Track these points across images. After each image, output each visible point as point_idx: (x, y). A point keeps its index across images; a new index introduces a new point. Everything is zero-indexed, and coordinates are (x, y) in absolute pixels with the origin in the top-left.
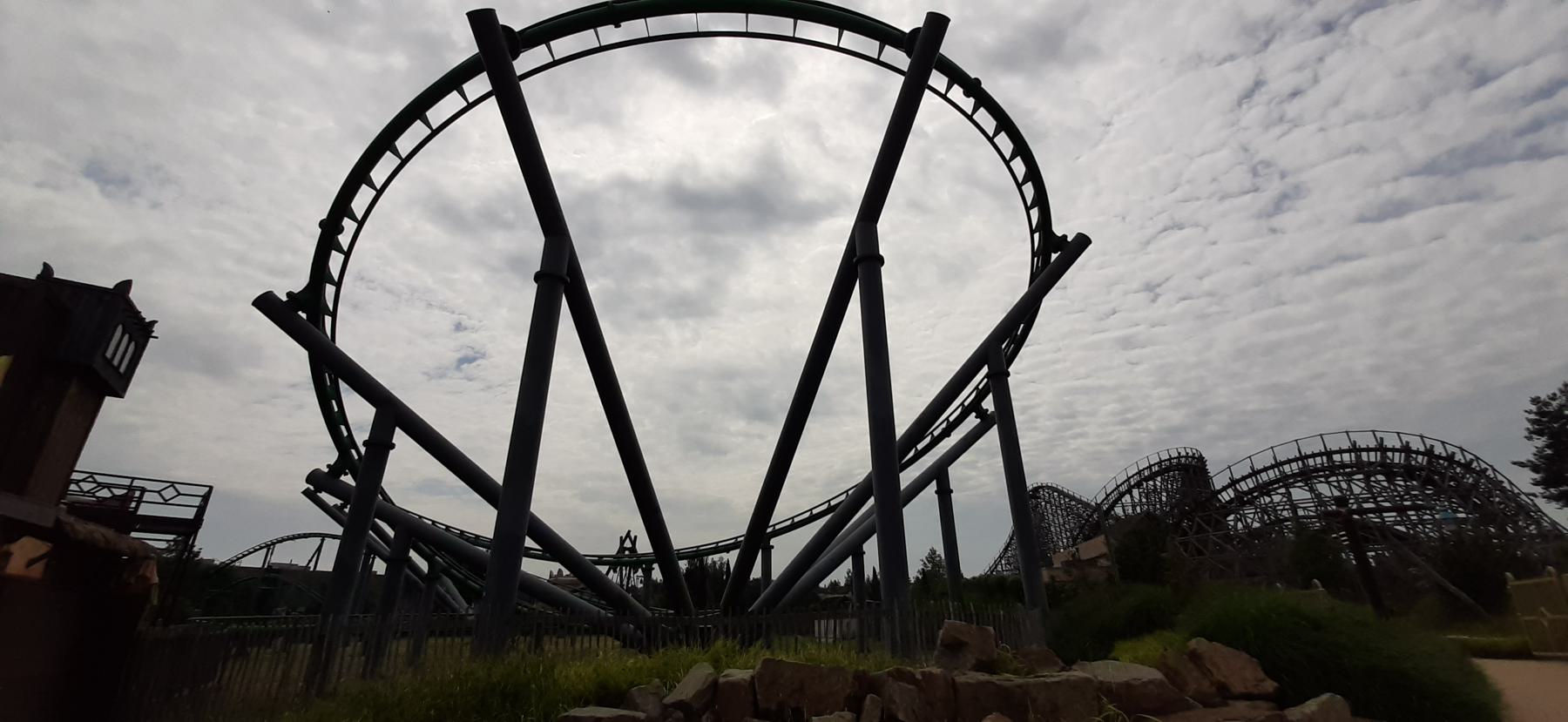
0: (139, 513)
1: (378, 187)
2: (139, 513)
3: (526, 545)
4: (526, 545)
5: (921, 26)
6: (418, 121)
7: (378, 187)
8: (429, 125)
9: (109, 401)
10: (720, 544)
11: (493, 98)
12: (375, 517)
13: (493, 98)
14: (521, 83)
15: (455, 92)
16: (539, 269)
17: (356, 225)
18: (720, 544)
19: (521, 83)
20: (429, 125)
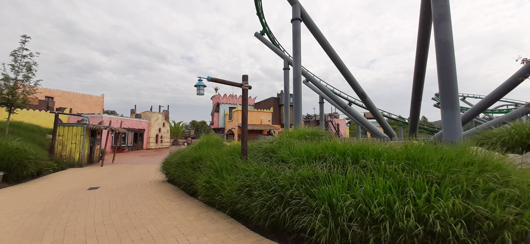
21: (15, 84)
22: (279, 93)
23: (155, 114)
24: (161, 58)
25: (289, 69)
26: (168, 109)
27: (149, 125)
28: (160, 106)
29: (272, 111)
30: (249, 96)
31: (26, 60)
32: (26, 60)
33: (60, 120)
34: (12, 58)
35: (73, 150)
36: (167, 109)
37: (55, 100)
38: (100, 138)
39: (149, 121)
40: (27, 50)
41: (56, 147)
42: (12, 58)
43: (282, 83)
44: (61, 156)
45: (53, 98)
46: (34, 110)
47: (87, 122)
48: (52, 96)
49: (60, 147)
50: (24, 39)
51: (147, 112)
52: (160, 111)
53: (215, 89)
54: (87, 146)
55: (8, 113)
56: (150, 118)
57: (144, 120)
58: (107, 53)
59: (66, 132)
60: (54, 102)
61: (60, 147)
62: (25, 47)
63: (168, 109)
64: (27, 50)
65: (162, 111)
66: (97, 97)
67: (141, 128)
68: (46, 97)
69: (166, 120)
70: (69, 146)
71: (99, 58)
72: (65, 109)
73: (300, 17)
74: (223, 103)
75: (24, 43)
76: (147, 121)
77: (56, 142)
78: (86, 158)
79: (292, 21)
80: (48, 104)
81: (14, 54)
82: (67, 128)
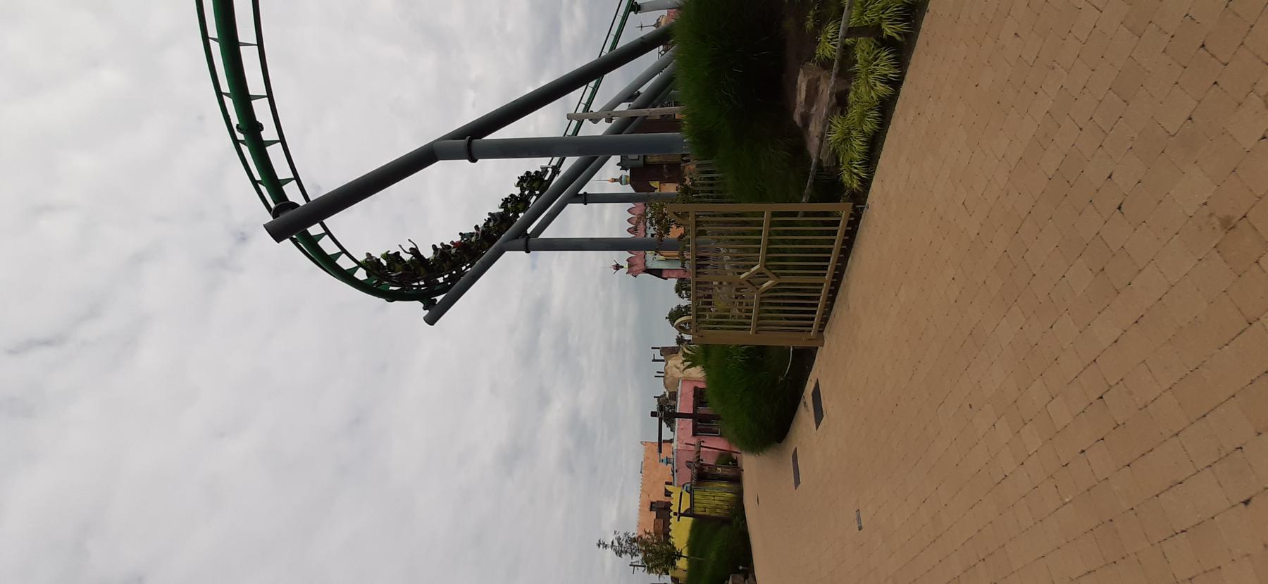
0: (229, 92)
1: (292, 176)
2: (229, 92)
3: (699, 368)
4: (699, 368)
5: (301, 205)
6: (319, 243)
7: (340, 251)
8: (289, 180)
9: (262, 133)
10: (258, 177)
11: (325, 221)
12: (435, 304)
13: (325, 221)
14: (318, 224)
15: (284, 187)
16: (467, 161)
17: (344, 255)
18: (258, 177)
19: (318, 224)
20: (289, 180)
21: (650, 551)
22: (619, 161)
23: (669, 370)
24: (539, 309)
25: (585, 193)
26: (659, 348)
27: (686, 380)
28: (654, 360)
29: (658, 182)
30: (630, 236)
31: (624, 543)
32: (624, 543)
33: (686, 511)
34: (623, 555)
35: (722, 499)
36: (659, 350)
37: (654, 500)
38: (707, 467)
39: (681, 381)
40: (613, 543)
41: (717, 515)
42: (623, 555)
43: (609, 206)
44: (728, 509)
45: (652, 503)
46: (671, 524)
47: (689, 485)
48: (650, 503)
49: (718, 511)
50: (601, 546)
51: (664, 382)
52: (663, 361)
53: (617, 269)
54: (717, 484)
55: (682, 558)
56: (674, 378)
57: (679, 388)
58: (544, 400)
59: (700, 505)
60: (658, 501)
61: (718, 511)
62: (610, 544)
63: (659, 348)
64: (613, 543)
65: (662, 358)
66: (646, 451)
67: (691, 394)
68: (651, 510)
69: (677, 353)
70: (717, 502)
71: (556, 413)
72: (666, 489)
73: (463, 140)
74: (645, 264)
75: (606, 546)
76: (680, 383)
77: (713, 515)
78: (732, 486)
79: (473, 160)
80: (662, 508)
81: (619, 553)
82: (695, 505)
